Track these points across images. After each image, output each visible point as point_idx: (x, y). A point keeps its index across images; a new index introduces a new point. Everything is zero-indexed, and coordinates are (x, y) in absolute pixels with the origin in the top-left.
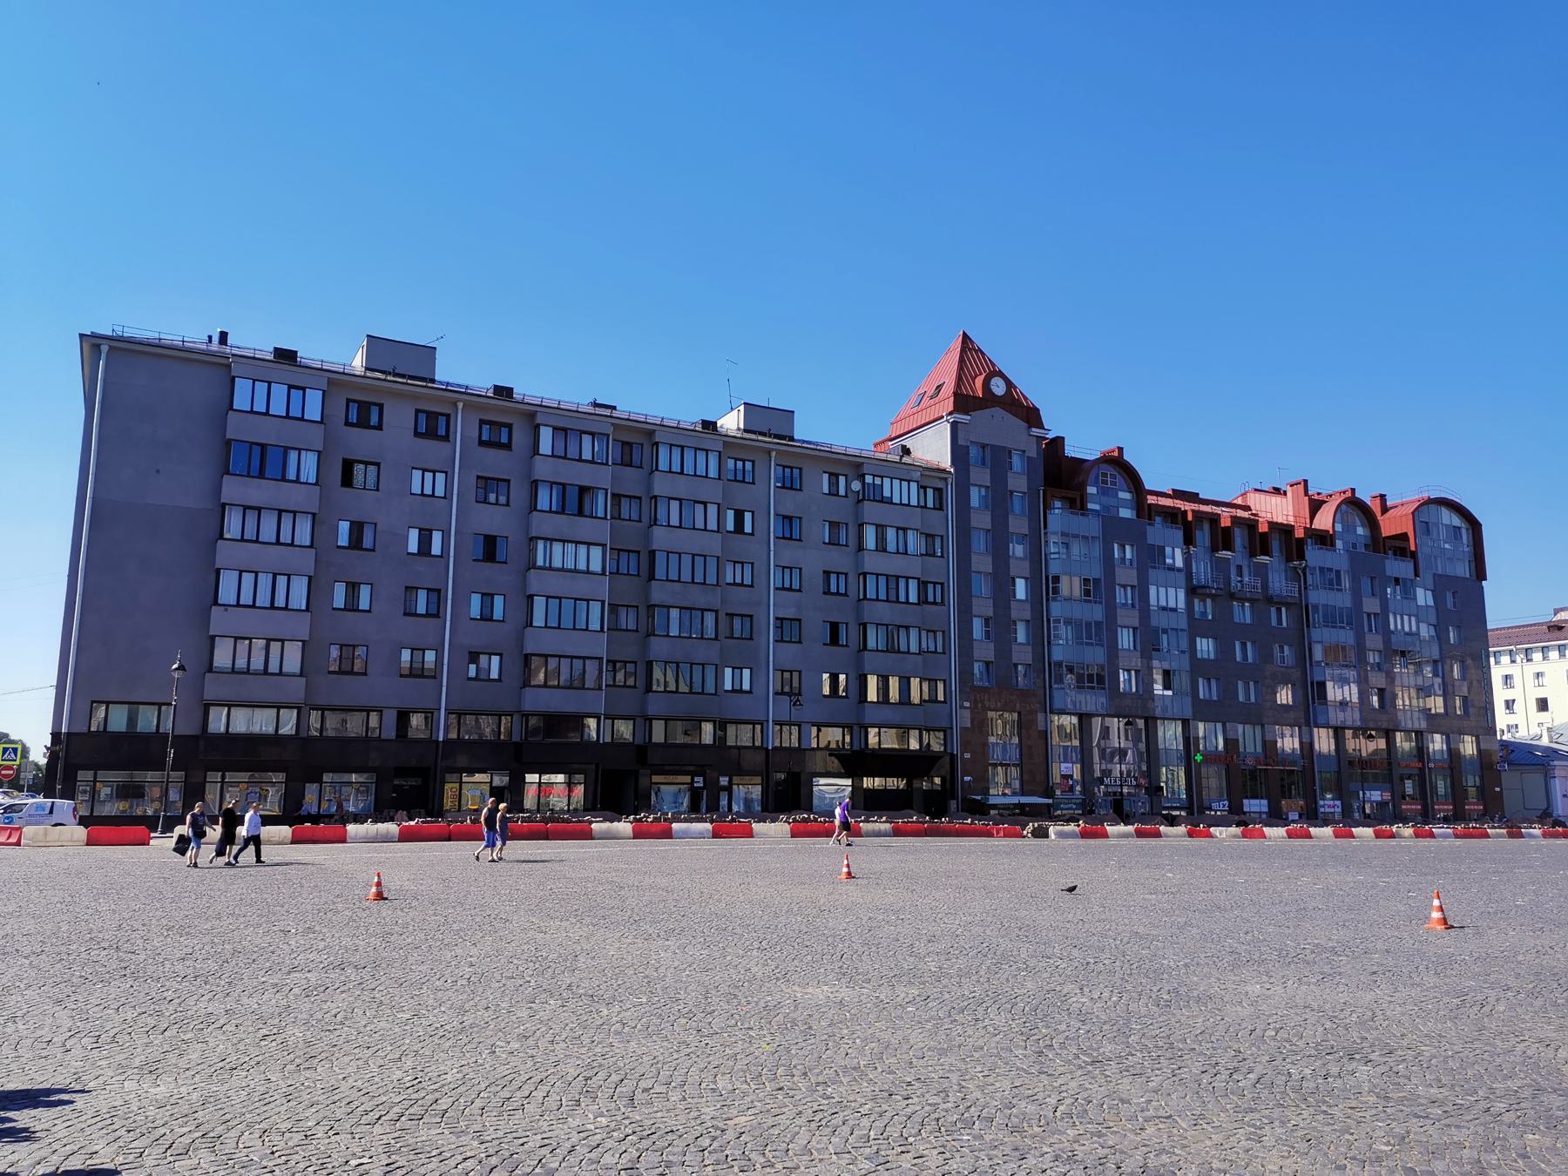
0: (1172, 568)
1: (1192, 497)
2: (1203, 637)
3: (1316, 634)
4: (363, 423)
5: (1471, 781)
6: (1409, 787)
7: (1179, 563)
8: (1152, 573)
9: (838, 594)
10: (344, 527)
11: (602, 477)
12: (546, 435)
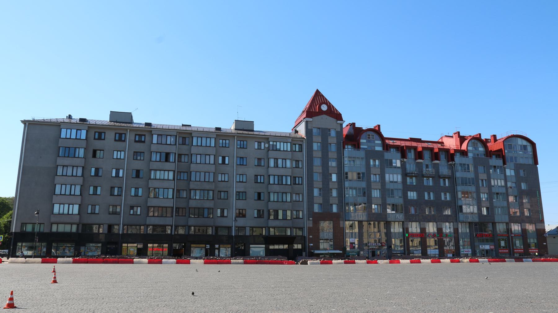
0: (396, 167)
1: (419, 140)
2: (411, 191)
3: (459, 188)
4: (100, 138)
5: (532, 241)
6: (503, 243)
7: (399, 165)
8: (387, 170)
9: (261, 182)
10: (93, 170)
11: (172, 149)
12: (155, 137)
